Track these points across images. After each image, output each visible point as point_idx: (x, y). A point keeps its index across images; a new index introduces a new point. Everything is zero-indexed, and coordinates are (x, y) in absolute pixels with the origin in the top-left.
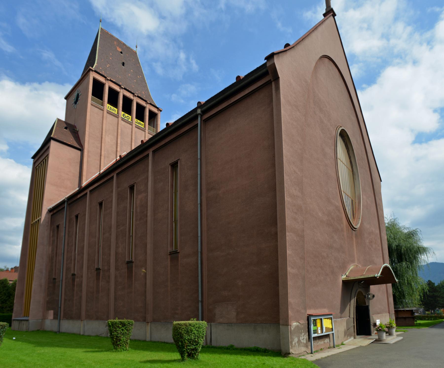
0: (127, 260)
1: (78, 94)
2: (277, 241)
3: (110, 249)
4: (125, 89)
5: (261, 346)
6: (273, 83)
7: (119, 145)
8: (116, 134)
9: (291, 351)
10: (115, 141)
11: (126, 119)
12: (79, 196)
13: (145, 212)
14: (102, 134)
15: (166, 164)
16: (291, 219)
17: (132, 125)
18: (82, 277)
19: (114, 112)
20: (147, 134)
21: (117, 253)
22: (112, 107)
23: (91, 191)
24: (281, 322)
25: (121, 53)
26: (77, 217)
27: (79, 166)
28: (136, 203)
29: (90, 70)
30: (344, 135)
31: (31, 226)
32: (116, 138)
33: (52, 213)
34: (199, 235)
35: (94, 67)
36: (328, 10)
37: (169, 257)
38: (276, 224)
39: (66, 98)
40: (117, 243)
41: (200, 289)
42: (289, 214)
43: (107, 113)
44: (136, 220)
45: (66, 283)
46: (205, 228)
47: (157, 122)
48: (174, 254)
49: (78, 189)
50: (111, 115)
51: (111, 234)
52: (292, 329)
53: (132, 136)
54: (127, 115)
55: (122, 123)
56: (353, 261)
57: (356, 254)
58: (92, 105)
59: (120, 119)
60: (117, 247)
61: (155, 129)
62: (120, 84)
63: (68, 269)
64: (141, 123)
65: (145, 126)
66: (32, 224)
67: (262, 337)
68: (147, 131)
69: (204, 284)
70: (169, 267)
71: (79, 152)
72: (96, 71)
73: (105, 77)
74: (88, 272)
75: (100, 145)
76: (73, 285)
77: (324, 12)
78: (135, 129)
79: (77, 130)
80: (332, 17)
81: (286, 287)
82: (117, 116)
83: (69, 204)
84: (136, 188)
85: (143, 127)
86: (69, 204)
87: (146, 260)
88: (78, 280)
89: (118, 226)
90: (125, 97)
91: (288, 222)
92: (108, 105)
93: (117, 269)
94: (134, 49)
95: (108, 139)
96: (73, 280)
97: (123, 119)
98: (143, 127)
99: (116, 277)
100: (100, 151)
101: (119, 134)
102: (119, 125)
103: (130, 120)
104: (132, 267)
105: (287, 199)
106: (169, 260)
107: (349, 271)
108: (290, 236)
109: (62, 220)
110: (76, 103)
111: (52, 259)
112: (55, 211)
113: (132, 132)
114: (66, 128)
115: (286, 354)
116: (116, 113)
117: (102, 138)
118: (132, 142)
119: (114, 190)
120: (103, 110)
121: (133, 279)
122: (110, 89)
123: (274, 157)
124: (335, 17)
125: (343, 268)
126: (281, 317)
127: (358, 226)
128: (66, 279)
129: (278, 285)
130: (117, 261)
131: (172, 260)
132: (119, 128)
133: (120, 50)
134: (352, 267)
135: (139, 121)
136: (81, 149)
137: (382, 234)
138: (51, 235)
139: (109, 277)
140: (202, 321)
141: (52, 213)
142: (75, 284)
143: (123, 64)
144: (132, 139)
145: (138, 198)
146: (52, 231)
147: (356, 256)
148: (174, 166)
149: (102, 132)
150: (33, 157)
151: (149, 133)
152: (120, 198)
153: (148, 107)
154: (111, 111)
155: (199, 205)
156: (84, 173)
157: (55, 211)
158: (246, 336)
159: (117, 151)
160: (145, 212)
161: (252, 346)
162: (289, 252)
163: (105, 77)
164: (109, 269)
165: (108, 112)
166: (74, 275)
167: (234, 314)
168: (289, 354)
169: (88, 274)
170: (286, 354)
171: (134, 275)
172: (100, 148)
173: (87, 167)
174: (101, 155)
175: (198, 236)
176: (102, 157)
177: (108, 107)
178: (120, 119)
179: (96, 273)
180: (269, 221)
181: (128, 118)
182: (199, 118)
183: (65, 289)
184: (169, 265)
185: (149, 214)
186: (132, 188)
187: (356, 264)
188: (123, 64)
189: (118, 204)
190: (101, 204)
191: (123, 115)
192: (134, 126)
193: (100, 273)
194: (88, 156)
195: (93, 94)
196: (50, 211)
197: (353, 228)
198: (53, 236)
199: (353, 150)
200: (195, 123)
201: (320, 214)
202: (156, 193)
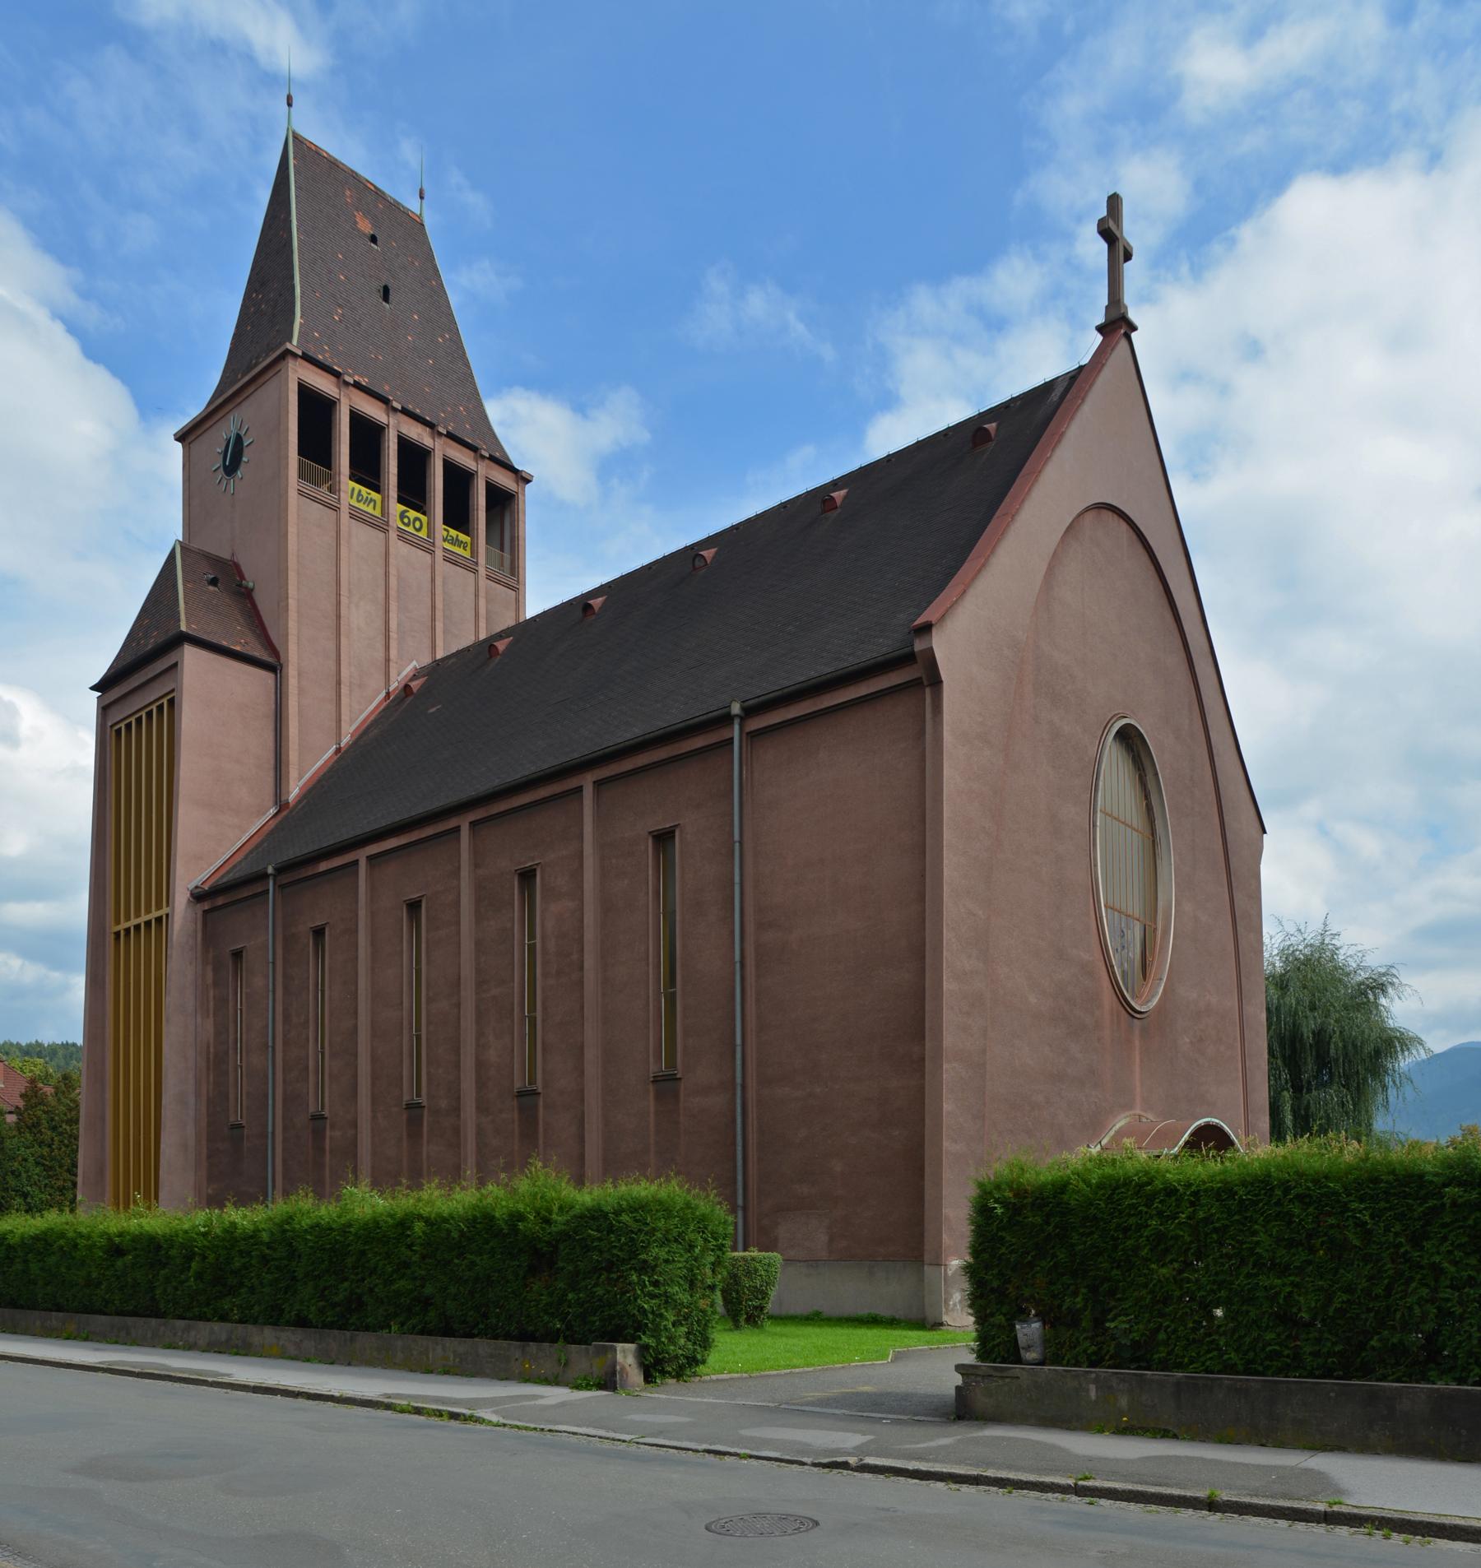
0: (518, 1085)
1: (239, 439)
2: (923, 1076)
3: (457, 1050)
4: (405, 412)
5: (884, 1312)
6: (928, 690)
7: (393, 635)
8: (381, 595)
9: (945, 1318)
10: (379, 623)
11: (410, 529)
12: (323, 866)
13: (575, 957)
14: (338, 603)
15: (639, 827)
16: (955, 1030)
17: (432, 553)
18: (354, 1124)
19: (370, 509)
20: (483, 582)
21: (480, 1065)
22: (364, 490)
23: (370, 858)
24: (927, 1258)
25: (374, 239)
26: (319, 933)
27: (272, 727)
28: (543, 926)
29: (288, 352)
30: (1129, 738)
31: (111, 939)
32: (381, 613)
33: (206, 906)
34: (739, 1041)
35: (295, 342)
36: (1114, 315)
37: (651, 1087)
38: (924, 1038)
39: (181, 437)
40: (480, 1034)
41: (740, 1178)
42: (949, 1018)
43: (352, 516)
44: (545, 975)
45: (285, 1140)
46: (752, 1023)
47: (515, 525)
48: (666, 1084)
49: (272, 811)
50: (364, 522)
51: (458, 1005)
52: (950, 1273)
53: (433, 594)
54: (412, 514)
55: (399, 549)
56: (1128, 1106)
57: (1138, 1084)
58: (300, 493)
59: (393, 535)
60: (481, 1047)
61: (507, 555)
62: (385, 389)
63: (292, 1100)
64: (463, 537)
65: (474, 552)
66: (117, 934)
67: (886, 1290)
68: (482, 571)
69: (750, 1165)
70: (652, 1116)
71: (267, 677)
72: (306, 358)
73: (337, 375)
74: (373, 1111)
75: (332, 646)
76: (320, 1149)
77: (1100, 319)
78: (442, 567)
79: (251, 585)
80: (1123, 343)
81: (938, 1184)
82: (380, 524)
83: (282, 887)
84: (542, 879)
85: (467, 554)
86: (282, 887)
87: (582, 1091)
88: (338, 1133)
89: (480, 984)
90: (404, 444)
91: (948, 1040)
92: (352, 484)
93: (482, 1108)
94: (413, 204)
95: (360, 617)
96: (318, 1135)
97: (403, 536)
98: (467, 554)
99: (480, 1132)
100: (334, 668)
101: (393, 593)
102: (392, 560)
103: (423, 534)
104: (536, 1107)
105: (948, 985)
106: (652, 1095)
107: (1112, 1133)
108: (951, 1073)
109: (259, 933)
110: (231, 468)
111: (217, 1063)
112: (220, 898)
113: (433, 580)
114: (214, 582)
115: (938, 1325)
116: (378, 513)
117: (338, 617)
118: (433, 619)
119: (465, 872)
120: (336, 509)
121: (541, 1142)
122: (357, 419)
123: (923, 876)
124: (1134, 335)
125: (1094, 1126)
126: (928, 1246)
127: (1148, 1004)
128: (285, 1128)
129: (922, 1176)
130: (481, 1084)
131: (659, 1097)
132: (393, 571)
133: (366, 227)
134: (1121, 1123)
135: (453, 533)
136: (273, 665)
137: (1248, 1010)
138: (210, 980)
139: (457, 1131)
140: (745, 1250)
141: (206, 906)
142: (327, 1147)
143: (386, 294)
144: (433, 608)
145: (549, 913)
146: (209, 968)
147: (1138, 1090)
148: (663, 839)
149: (338, 595)
150: (101, 687)
151: (488, 578)
152: (486, 900)
153: (484, 472)
154: (361, 506)
155: (738, 966)
156: (293, 755)
157: (220, 901)
158: (850, 1288)
159: (388, 660)
160: (575, 957)
161: (863, 1312)
162: (947, 1107)
163: (337, 375)
164: (456, 1110)
165: (356, 515)
166: (318, 1118)
167: (823, 1238)
168: (942, 1324)
169: (374, 1117)
170: (938, 1325)
171: (541, 1130)
172: (333, 656)
173: (300, 731)
174: (339, 683)
175: (734, 1046)
176: (344, 690)
177: (349, 488)
178: (393, 535)
179: (405, 1117)
180: (909, 1031)
181: (417, 524)
182: (736, 727)
183: (284, 1161)
184: (652, 1109)
185: (590, 962)
186: (527, 876)
187: (1138, 1112)
188: (386, 294)
189: (479, 918)
190: (414, 906)
191: (402, 515)
192: (439, 554)
193: (422, 1116)
194: (301, 691)
195: (302, 452)
196: (198, 896)
197: (1132, 1012)
198: (216, 984)
199: (1156, 774)
200: (724, 734)
201: (1033, 999)
202: (607, 907)
